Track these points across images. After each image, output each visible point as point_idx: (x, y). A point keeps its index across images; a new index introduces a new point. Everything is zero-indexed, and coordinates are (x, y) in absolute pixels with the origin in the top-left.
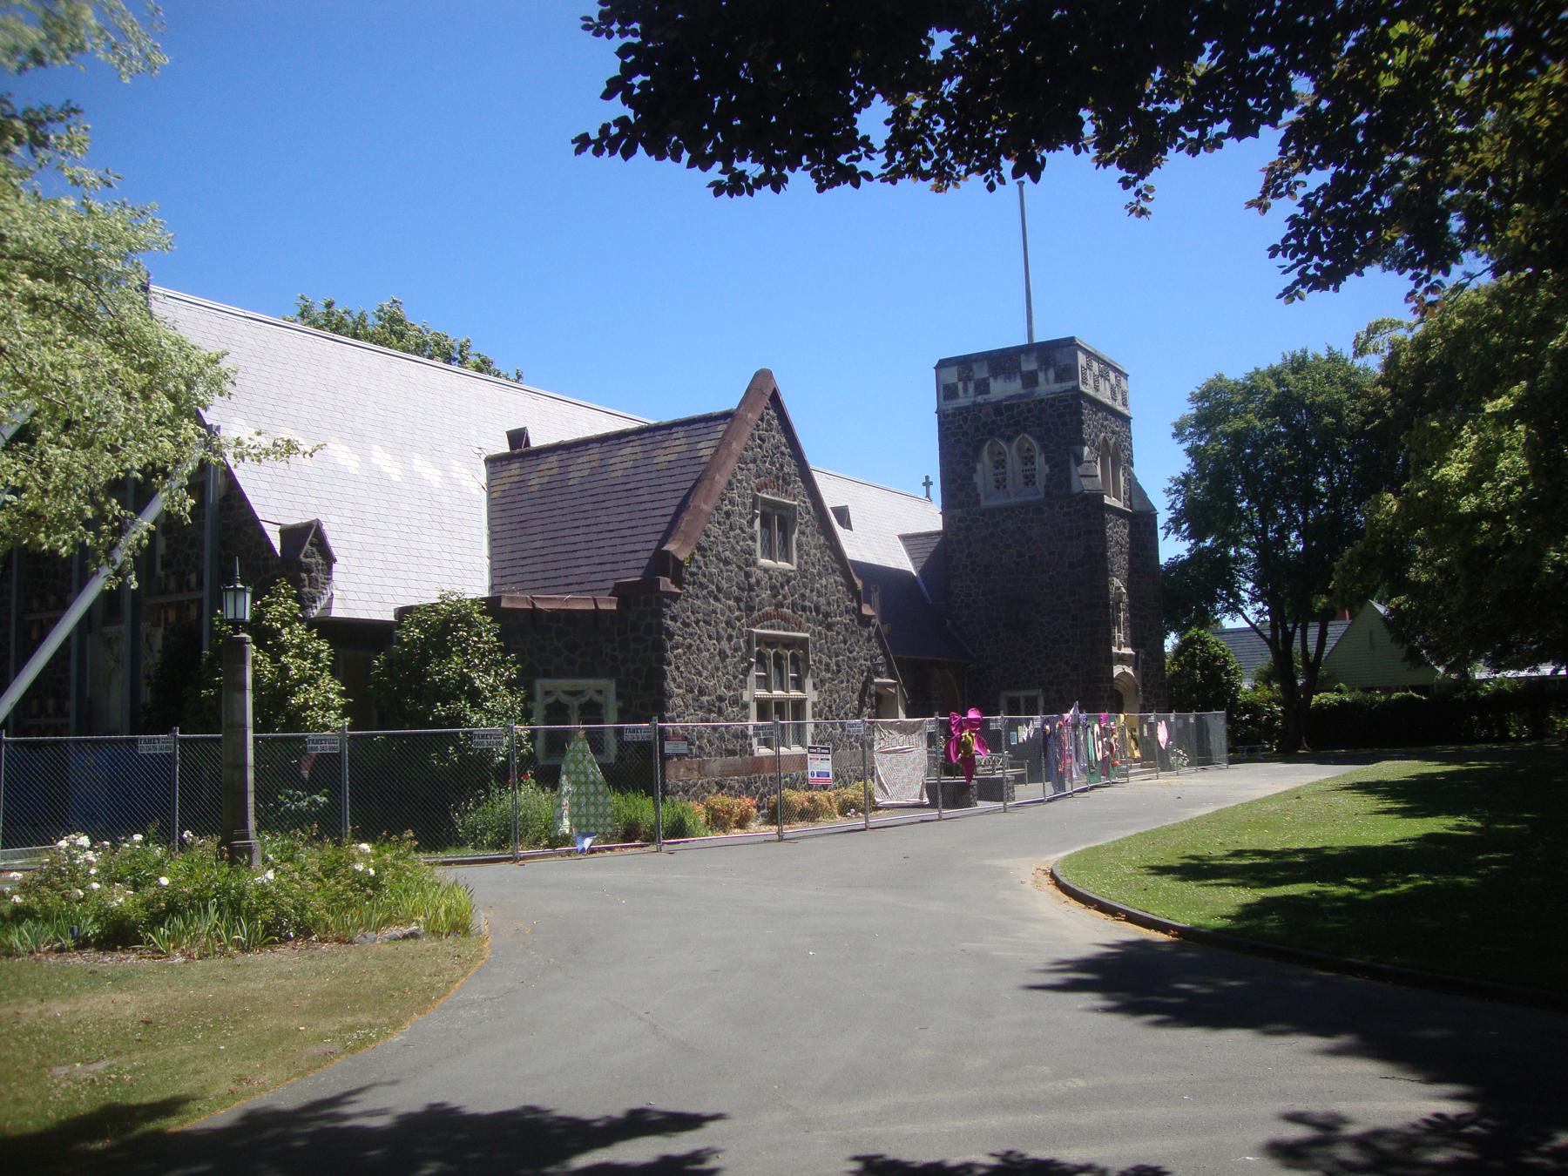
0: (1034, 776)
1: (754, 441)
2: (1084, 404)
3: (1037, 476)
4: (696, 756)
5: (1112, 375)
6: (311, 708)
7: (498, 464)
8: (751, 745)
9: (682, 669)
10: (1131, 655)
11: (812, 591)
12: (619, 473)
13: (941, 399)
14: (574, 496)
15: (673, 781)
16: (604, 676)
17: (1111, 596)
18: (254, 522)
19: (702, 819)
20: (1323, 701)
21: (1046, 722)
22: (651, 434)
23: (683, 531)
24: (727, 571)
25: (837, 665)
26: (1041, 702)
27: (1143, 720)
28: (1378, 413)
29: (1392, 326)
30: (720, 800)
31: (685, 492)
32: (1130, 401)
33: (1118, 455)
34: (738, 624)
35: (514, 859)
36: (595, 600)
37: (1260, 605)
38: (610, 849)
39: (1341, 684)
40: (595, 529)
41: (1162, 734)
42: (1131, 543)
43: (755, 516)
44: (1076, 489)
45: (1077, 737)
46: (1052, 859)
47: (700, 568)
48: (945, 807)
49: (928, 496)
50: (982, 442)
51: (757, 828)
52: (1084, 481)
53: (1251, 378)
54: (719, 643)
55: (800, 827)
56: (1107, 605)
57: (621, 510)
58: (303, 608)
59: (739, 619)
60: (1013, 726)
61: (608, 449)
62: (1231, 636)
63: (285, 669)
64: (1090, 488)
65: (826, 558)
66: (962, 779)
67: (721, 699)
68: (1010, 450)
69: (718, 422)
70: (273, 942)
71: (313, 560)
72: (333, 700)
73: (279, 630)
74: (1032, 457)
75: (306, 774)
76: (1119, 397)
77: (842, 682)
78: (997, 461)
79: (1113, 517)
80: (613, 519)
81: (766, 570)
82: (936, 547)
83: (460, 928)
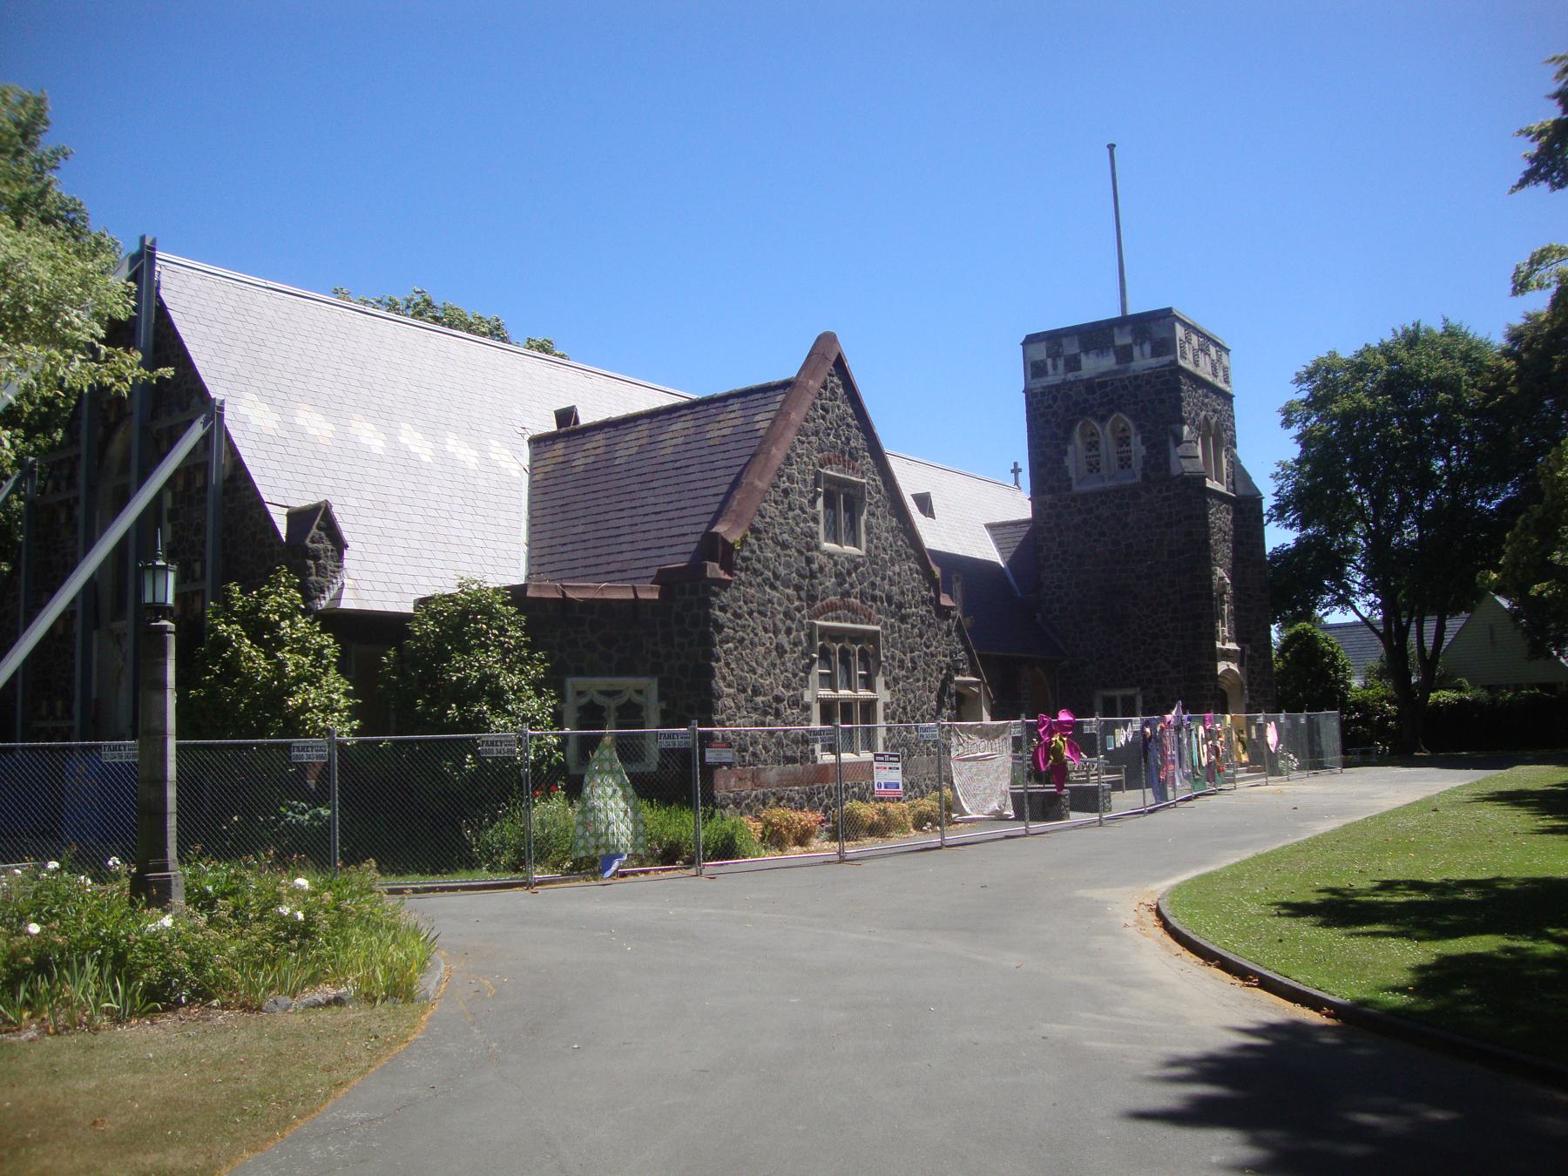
0: (1132, 783)
1: (816, 411)
2: (1183, 381)
3: (1133, 459)
4: (750, 765)
5: (1213, 350)
6: (310, 710)
7: (542, 444)
8: (813, 751)
9: (733, 665)
10: (1235, 651)
11: (883, 579)
12: (669, 450)
13: (1029, 377)
14: (619, 476)
15: (723, 792)
16: (644, 674)
17: (1214, 587)
18: (260, 503)
19: (757, 836)
20: (1441, 700)
21: (1146, 724)
22: (705, 408)
23: (733, 511)
24: (786, 555)
25: (912, 660)
26: (1139, 703)
27: (1250, 721)
28: (1501, 388)
29: (1561, 255)
30: (778, 814)
31: (738, 469)
32: (1232, 378)
33: (1220, 436)
34: (798, 615)
35: (526, 885)
36: (634, 588)
37: (1371, 597)
38: (646, 872)
39: (1464, 680)
40: (641, 511)
41: (1272, 736)
42: (1235, 530)
43: (817, 495)
44: (1175, 470)
45: (1180, 741)
46: (1159, 888)
47: (753, 552)
48: (1034, 818)
49: (1016, 483)
50: (1073, 423)
51: (822, 847)
52: (1184, 462)
53: (1361, 354)
54: (776, 637)
55: (870, 844)
56: (1210, 596)
57: (669, 490)
58: (308, 598)
59: (799, 609)
60: (1109, 729)
61: (657, 424)
62: (1338, 631)
63: (281, 665)
64: (1191, 470)
65: (900, 543)
66: (1051, 788)
67: (778, 699)
68: (1103, 428)
69: (777, 392)
70: (155, 1010)
71: (321, 546)
72: (338, 701)
73: (277, 624)
74: (1128, 437)
75: (312, 783)
76: (1221, 373)
77: (918, 680)
78: (1090, 443)
79: (1215, 502)
80: (661, 500)
81: (830, 555)
82: (1022, 542)
83: (400, 991)
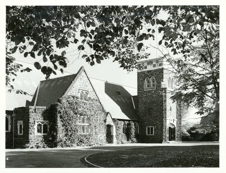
68: (150, 79)
